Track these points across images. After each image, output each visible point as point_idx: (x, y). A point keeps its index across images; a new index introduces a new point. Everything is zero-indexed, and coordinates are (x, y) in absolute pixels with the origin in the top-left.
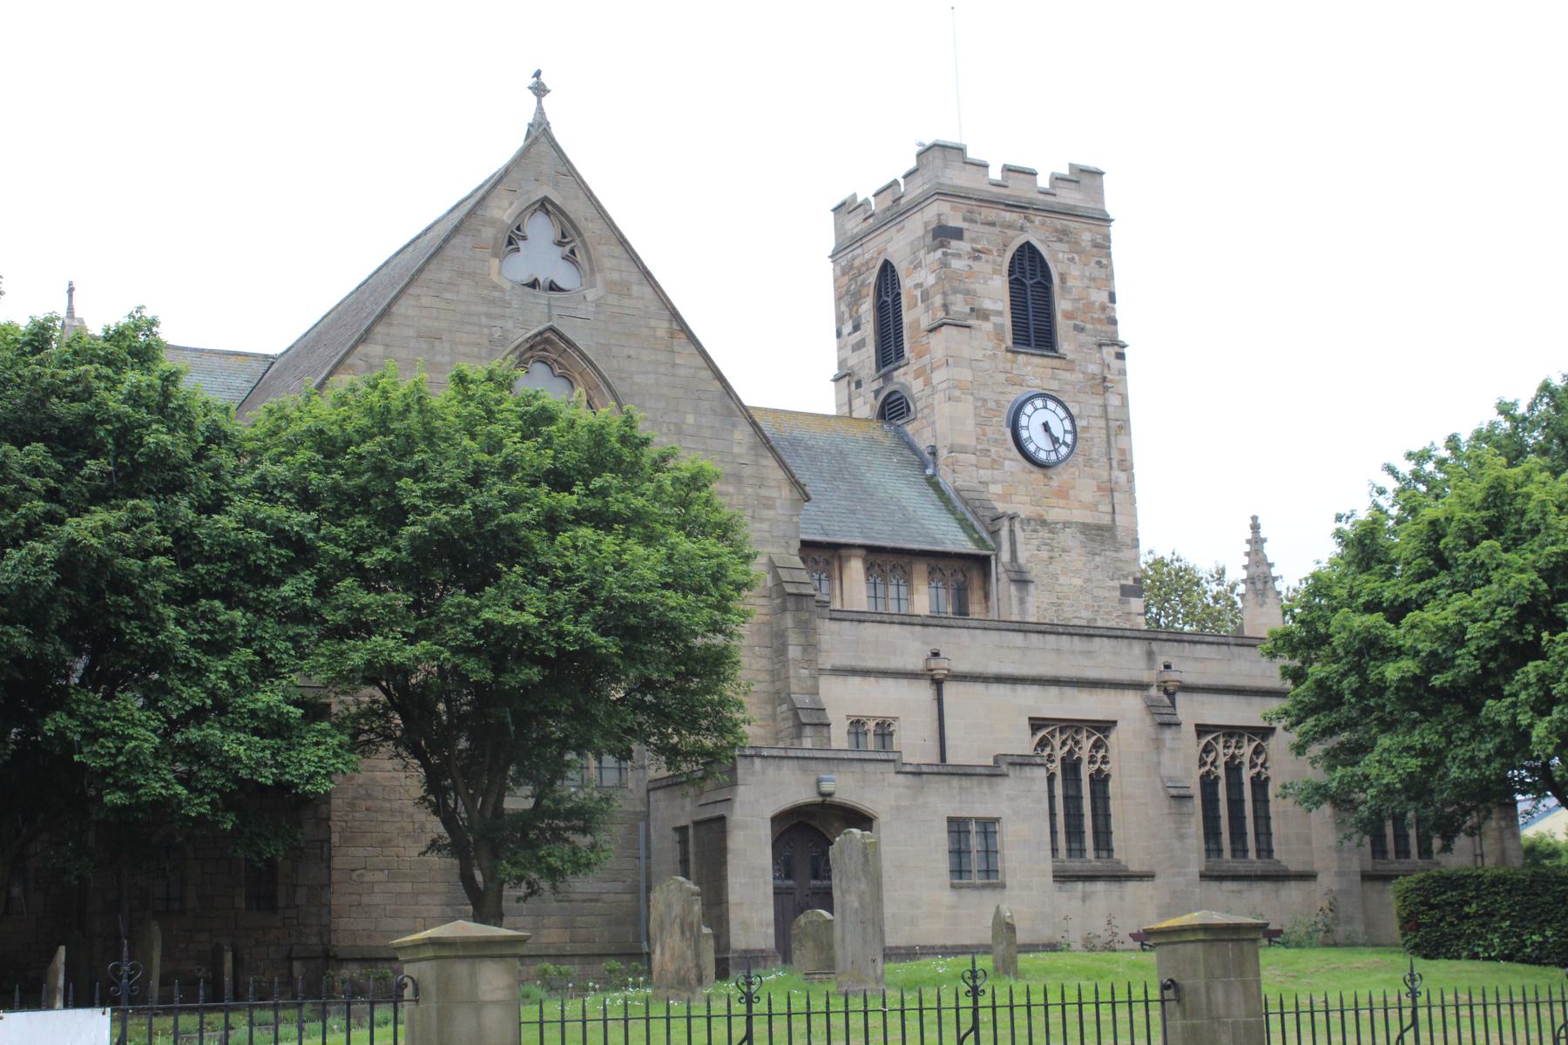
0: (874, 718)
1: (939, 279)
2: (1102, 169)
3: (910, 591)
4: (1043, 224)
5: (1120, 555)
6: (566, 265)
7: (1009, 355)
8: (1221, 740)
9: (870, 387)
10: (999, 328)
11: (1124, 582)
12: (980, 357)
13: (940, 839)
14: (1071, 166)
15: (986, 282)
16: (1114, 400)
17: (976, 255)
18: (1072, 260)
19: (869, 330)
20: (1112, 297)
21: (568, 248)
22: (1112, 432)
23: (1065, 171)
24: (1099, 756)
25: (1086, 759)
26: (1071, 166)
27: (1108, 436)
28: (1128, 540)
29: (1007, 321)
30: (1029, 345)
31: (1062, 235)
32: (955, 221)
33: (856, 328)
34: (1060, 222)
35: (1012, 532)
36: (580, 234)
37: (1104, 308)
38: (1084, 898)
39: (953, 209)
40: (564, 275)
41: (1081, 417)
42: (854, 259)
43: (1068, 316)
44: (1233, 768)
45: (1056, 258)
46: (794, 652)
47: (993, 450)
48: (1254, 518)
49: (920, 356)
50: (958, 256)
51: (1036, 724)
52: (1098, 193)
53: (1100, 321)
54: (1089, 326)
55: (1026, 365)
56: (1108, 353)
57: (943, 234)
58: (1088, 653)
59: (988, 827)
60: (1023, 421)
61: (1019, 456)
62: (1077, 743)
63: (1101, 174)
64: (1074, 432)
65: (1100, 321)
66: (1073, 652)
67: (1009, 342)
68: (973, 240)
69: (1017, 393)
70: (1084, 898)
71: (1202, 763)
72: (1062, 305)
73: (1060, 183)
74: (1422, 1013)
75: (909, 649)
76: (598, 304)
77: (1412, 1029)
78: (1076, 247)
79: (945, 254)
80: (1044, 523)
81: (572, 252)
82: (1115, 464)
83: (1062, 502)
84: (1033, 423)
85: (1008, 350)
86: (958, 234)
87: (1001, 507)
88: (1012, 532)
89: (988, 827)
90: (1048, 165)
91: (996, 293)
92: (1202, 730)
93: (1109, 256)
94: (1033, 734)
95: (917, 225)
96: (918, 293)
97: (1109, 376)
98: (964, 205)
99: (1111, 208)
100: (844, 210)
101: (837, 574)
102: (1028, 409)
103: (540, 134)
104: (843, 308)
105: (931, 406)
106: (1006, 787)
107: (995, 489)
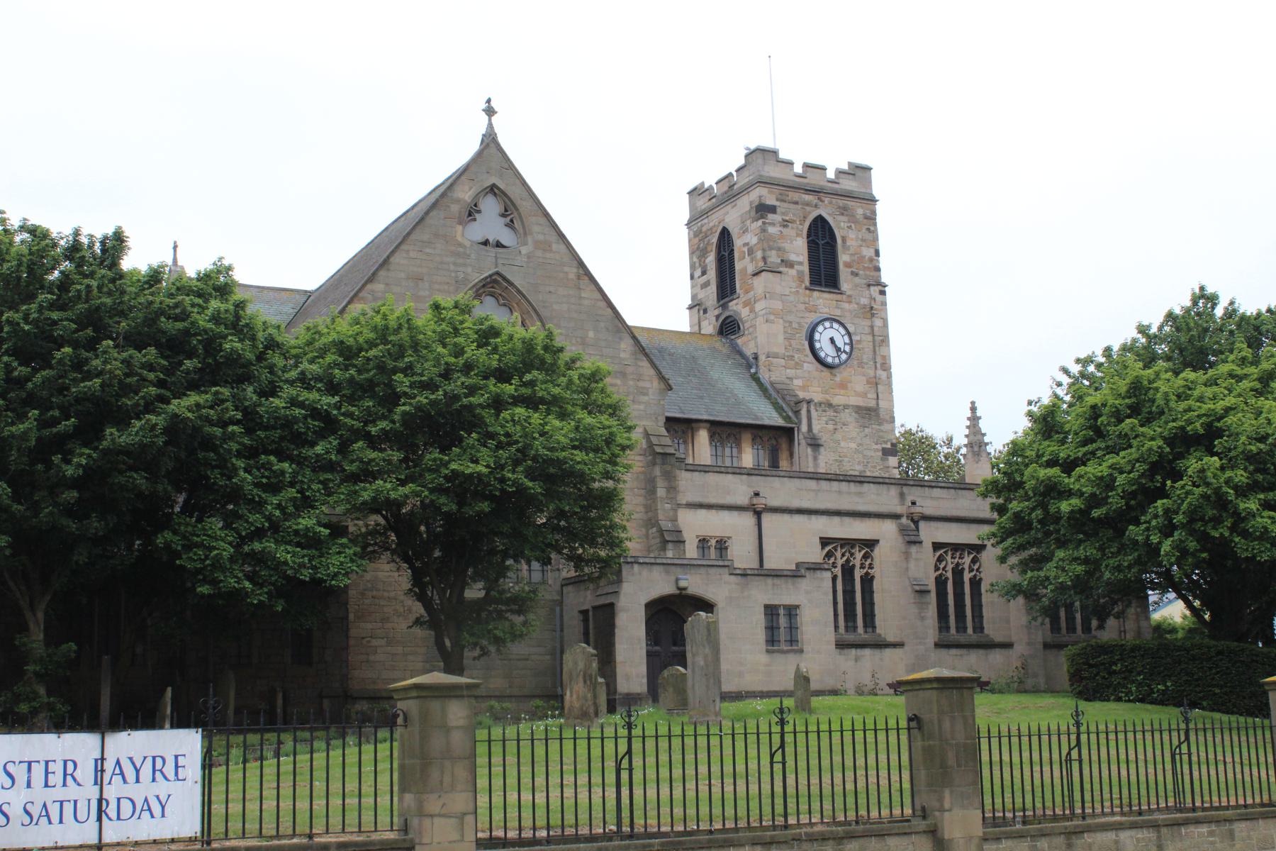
0: (715, 537)
1: (760, 240)
2: (870, 165)
3: (740, 452)
4: (831, 203)
5: (882, 428)
6: (507, 230)
7: (808, 292)
8: (950, 553)
9: (713, 313)
10: (800, 274)
11: (884, 446)
12: (787, 293)
13: (759, 619)
14: (850, 164)
15: (791, 242)
16: (878, 323)
17: (785, 223)
18: (850, 227)
19: (712, 274)
20: (877, 253)
21: (509, 218)
22: (877, 344)
23: (845, 167)
24: (867, 563)
25: (858, 566)
26: (850, 164)
27: (874, 347)
28: (887, 417)
29: (806, 268)
30: (821, 285)
31: (844, 210)
32: (771, 200)
33: (704, 273)
34: (841, 202)
35: (809, 411)
36: (517, 209)
37: (871, 260)
38: (857, 659)
39: (769, 192)
40: (506, 237)
41: (855, 334)
42: (702, 226)
43: (848, 265)
44: (958, 572)
45: (840, 226)
46: (661, 492)
47: (796, 356)
48: (973, 403)
49: (747, 292)
50: (773, 224)
51: (825, 542)
52: (868, 182)
53: (868, 268)
54: (861, 272)
55: (818, 298)
56: (874, 291)
57: (763, 210)
58: (860, 494)
59: (792, 611)
60: (817, 336)
61: (814, 361)
62: (852, 554)
63: (870, 169)
64: (851, 344)
65: (868, 268)
66: (849, 493)
67: (807, 283)
68: (783, 214)
69: (814, 318)
70: (857, 659)
71: (937, 569)
72: (843, 258)
73: (842, 175)
74: (1084, 737)
75: (739, 490)
76: (529, 257)
77: (627, 757)
78: (853, 219)
79: (764, 223)
80: (830, 405)
81: (512, 221)
82: (878, 366)
83: (842, 392)
84: (823, 338)
85: (806, 288)
86: (773, 209)
87: (801, 395)
88: (809, 411)
89: (792, 611)
90: (834, 162)
91: (798, 249)
92: (937, 546)
93: (875, 225)
94: (823, 548)
95: (745, 203)
96: (746, 249)
97: (875, 306)
98: (777, 190)
99: (876, 191)
100: (695, 193)
101: (690, 440)
102: (820, 328)
103: (490, 141)
104: (695, 259)
105: (754, 326)
106: (804, 584)
107: (797, 382)
